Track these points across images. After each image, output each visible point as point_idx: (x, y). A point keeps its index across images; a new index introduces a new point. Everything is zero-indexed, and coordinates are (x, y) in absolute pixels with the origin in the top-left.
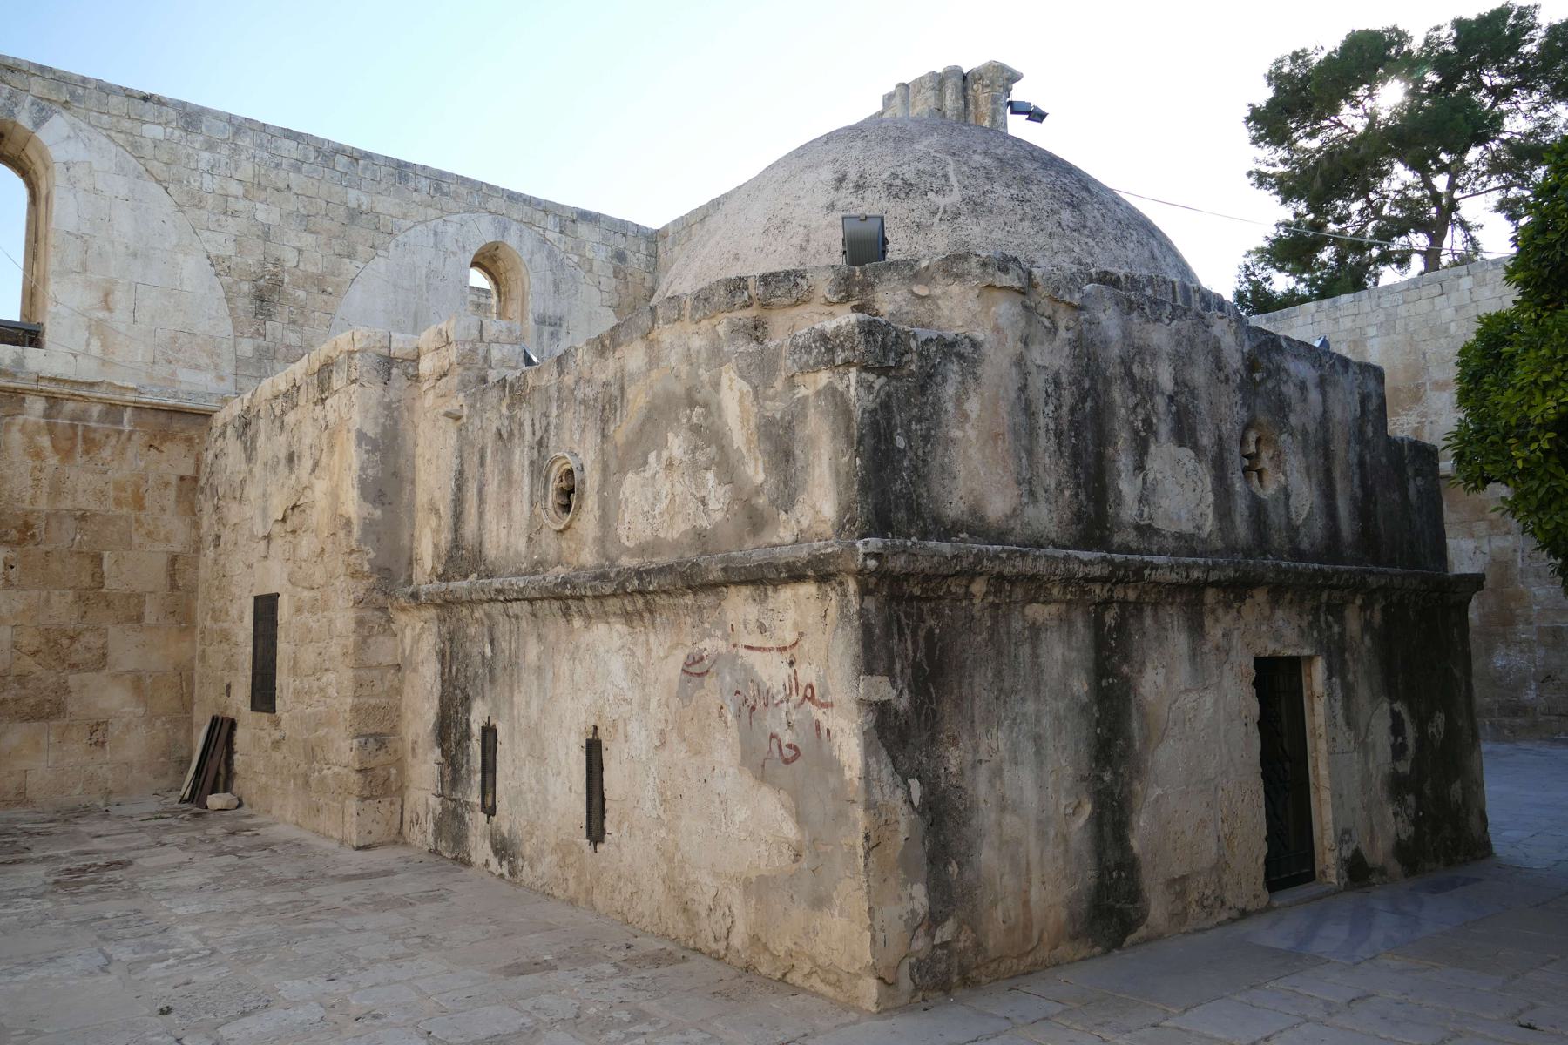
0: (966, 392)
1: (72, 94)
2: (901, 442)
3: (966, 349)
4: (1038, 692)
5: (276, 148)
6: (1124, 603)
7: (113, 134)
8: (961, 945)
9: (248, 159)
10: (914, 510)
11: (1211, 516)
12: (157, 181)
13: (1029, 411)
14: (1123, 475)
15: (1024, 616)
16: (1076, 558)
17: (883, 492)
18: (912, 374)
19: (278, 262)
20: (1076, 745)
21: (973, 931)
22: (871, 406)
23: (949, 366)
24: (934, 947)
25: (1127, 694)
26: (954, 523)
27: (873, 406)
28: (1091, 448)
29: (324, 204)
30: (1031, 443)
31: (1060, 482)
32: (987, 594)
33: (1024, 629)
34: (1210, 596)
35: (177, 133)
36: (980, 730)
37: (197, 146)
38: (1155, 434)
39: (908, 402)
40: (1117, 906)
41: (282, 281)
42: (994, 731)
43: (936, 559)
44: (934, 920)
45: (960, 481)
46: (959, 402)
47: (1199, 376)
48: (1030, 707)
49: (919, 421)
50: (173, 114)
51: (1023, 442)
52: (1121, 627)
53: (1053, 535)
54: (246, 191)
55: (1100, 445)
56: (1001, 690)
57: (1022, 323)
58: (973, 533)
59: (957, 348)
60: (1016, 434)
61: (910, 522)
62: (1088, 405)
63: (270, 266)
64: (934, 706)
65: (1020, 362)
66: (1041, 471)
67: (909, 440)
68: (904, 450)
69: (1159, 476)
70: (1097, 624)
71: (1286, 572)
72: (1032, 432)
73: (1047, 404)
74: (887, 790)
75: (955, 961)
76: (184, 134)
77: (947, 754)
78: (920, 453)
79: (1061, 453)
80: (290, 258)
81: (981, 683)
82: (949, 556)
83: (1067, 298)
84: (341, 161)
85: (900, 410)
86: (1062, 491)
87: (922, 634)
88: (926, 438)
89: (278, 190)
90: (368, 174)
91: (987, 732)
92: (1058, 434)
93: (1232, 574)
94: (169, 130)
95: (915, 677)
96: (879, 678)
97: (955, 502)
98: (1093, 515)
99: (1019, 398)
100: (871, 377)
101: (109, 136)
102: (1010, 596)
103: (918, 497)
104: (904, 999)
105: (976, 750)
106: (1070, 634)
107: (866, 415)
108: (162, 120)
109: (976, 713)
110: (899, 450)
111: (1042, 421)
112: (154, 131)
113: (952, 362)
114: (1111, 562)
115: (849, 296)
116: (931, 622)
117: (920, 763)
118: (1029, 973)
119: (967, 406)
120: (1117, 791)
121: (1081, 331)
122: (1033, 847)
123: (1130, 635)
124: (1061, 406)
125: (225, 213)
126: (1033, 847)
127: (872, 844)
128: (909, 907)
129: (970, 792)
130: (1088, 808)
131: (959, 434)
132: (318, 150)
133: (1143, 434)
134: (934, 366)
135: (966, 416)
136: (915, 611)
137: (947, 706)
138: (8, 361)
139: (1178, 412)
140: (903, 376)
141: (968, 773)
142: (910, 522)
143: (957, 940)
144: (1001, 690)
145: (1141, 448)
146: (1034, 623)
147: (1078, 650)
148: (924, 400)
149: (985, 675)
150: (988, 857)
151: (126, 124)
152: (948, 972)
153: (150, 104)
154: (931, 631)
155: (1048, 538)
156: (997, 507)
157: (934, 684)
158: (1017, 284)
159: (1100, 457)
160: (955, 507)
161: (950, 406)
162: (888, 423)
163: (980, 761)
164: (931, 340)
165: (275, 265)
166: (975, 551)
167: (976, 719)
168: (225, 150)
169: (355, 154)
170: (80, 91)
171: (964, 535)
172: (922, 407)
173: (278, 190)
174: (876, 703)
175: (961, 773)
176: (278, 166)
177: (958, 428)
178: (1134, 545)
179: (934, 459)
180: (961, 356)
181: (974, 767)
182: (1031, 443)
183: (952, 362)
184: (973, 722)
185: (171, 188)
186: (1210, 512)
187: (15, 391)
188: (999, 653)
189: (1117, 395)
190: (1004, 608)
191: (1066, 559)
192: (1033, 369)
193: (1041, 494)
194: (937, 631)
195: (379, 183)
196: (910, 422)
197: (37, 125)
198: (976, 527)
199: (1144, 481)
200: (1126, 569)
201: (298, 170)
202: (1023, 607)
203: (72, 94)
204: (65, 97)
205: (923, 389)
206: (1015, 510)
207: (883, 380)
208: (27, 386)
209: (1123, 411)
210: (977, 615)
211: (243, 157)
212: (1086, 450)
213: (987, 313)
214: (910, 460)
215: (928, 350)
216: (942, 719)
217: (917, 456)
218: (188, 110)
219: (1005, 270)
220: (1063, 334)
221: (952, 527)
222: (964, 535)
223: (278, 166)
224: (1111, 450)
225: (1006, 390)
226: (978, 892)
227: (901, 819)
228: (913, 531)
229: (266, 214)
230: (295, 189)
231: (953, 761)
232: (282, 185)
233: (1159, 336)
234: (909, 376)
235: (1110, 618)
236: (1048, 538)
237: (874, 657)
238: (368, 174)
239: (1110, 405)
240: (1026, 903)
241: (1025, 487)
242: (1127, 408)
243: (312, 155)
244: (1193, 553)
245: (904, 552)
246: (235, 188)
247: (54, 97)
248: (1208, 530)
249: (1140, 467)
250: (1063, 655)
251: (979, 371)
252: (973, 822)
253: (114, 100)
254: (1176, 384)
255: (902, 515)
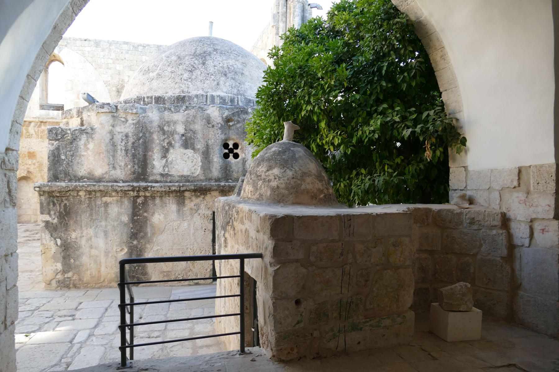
0: (88, 142)
1: (67, 43)
2: (63, 157)
3: (89, 131)
4: (106, 220)
5: (121, 48)
6: (145, 197)
7: (78, 51)
8: (74, 279)
9: (113, 52)
10: (67, 174)
11: (199, 170)
12: (90, 63)
13: (114, 145)
14: (156, 160)
15: (102, 201)
16: (118, 186)
17: (56, 170)
18: (69, 139)
19: (123, 80)
20: (122, 234)
21: (78, 276)
22: (52, 149)
23: (82, 136)
24: (65, 278)
25: (146, 221)
26: (82, 177)
27: (53, 149)
28: (141, 153)
29: (135, 62)
30: (114, 154)
31: (126, 164)
32: (85, 195)
33: (102, 203)
34: (187, 194)
35: (94, 48)
36: (84, 228)
37: (99, 51)
38: (173, 147)
39: (66, 147)
40: (137, 276)
41: (124, 86)
42: (89, 229)
43: (59, 187)
44: (64, 272)
45: (85, 166)
46: (85, 145)
47: (198, 126)
48: (103, 223)
49: (70, 151)
50: (92, 43)
51: (111, 154)
52: (144, 203)
53: (122, 178)
54: (113, 61)
55: (145, 152)
56: (92, 219)
57: (111, 121)
58: (88, 179)
59: (86, 131)
60: (108, 152)
61: (65, 177)
62: (141, 141)
63: (121, 82)
64: (67, 222)
65: (111, 133)
66: (118, 161)
67: (66, 156)
68: (64, 159)
69: (174, 159)
70: (134, 202)
71: (223, 187)
72: (115, 151)
73: (122, 142)
74: (48, 241)
75: (72, 282)
76: (96, 48)
77: (71, 234)
78: (70, 159)
79: (127, 156)
80: (126, 79)
81: (85, 218)
82: (64, 187)
83: (130, 112)
84: (140, 48)
85: (63, 149)
86: (127, 166)
87: (62, 205)
88: (72, 156)
89: (122, 60)
90: (149, 51)
91: (87, 229)
92: (126, 151)
93: (193, 188)
94: (92, 48)
95: (60, 215)
96: (46, 215)
97: (82, 171)
98: (140, 172)
99: (110, 142)
100: (53, 142)
101: (77, 52)
102: (95, 195)
103: (68, 171)
104: (54, 288)
105: (82, 233)
106: (121, 205)
107: (50, 152)
108: (90, 45)
109: (83, 224)
110: (62, 159)
111: (119, 147)
112: (88, 49)
113: (84, 135)
114: (133, 186)
115: (79, 116)
116: (66, 202)
117: (61, 235)
118: (99, 288)
119: (89, 146)
120: (139, 246)
121: (139, 120)
122: (103, 259)
123: (149, 205)
124: (128, 143)
125: (108, 69)
126: (103, 259)
127: (42, 253)
128: (55, 268)
129: (79, 243)
130: (126, 250)
131: (85, 153)
132: (133, 46)
133: (167, 147)
134: (76, 137)
135: (88, 149)
136: (60, 199)
137: (71, 222)
138: (55, 115)
139: (186, 139)
140: (65, 140)
141: (79, 239)
142: (65, 177)
143: (73, 277)
144: (92, 219)
145: (165, 152)
146: (106, 202)
147: (125, 209)
148: (72, 146)
149: (86, 215)
150: (85, 259)
151: (81, 48)
152: (69, 284)
153: (86, 41)
154: (66, 204)
155: (120, 179)
156: (99, 172)
157: (67, 217)
158: (108, 111)
159: (145, 156)
160: (82, 171)
161: (82, 147)
162: (58, 153)
163: (83, 236)
164: (76, 130)
165: (122, 81)
166: (74, 185)
167: (83, 226)
168: (107, 51)
169: (136, 45)
170: (69, 41)
171: (86, 180)
172: (71, 148)
173: (122, 60)
174: (45, 221)
175: (76, 238)
176: (122, 53)
177: (85, 152)
178: (159, 180)
179: (75, 161)
180: (87, 133)
181: (81, 237)
182: (114, 154)
183: (84, 135)
184: (82, 226)
185: (93, 64)
186: (199, 168)
187: (57, 122)
188: (92, 210)
189: (155, 136)
190: (93, 198)
191: (112, 186)
192: (117, 133)
193: (118, 167)
194: (68, 204)
195: (152, 53)
196: (66, 152)
197: (59, 52)
198: (91, 177)
199: (167, 161)
200: (139, 188)
201: (128, 53)
202: (101, 198)
203: (67, 43)
204: (66, 44)
205: (71, 143)
206: (106, 172)
207: (57, 142)
208: (59, 121)
209: (158, 141)
210: (83, 200)
211: (112, 52)
212: (139, 154)
213: (98, 120)
214: (66, 162)
215: (75, 133)
216: (70, 225)
217: (69, 160)
218: (97, 41)
219: (103, 108)
220: (130, 121)
221: (81, 178)
222: (86, 180)
223: (122, 53)
224: (150, 153)
225: (104, 140)
226: (81, 267)
227: (52, 247)
228: (66, 179)
229: (119, 67)
230: (127, 59)
231: (73, 235)
232: (123, 58)
233: (179, 117)
234: (67, 140)
235: (140, 201)
236: (120, 179)
237: (44, 210)
238: (149, 51)
239: (152, 141)
240: (99, 271)
241: (111, 166)
242: (160, 140)
243: (132, 48)
244: (189, 181)
245: (48, 186)
246: (110, 61)
247: (63, 44)
248: (198, 173)
249: (164, 156)
250: (118, 210)
251: (93, 136)
252: (80, 250)
253: (78, 42)
254: (186, 130)
255: (63, 175)
